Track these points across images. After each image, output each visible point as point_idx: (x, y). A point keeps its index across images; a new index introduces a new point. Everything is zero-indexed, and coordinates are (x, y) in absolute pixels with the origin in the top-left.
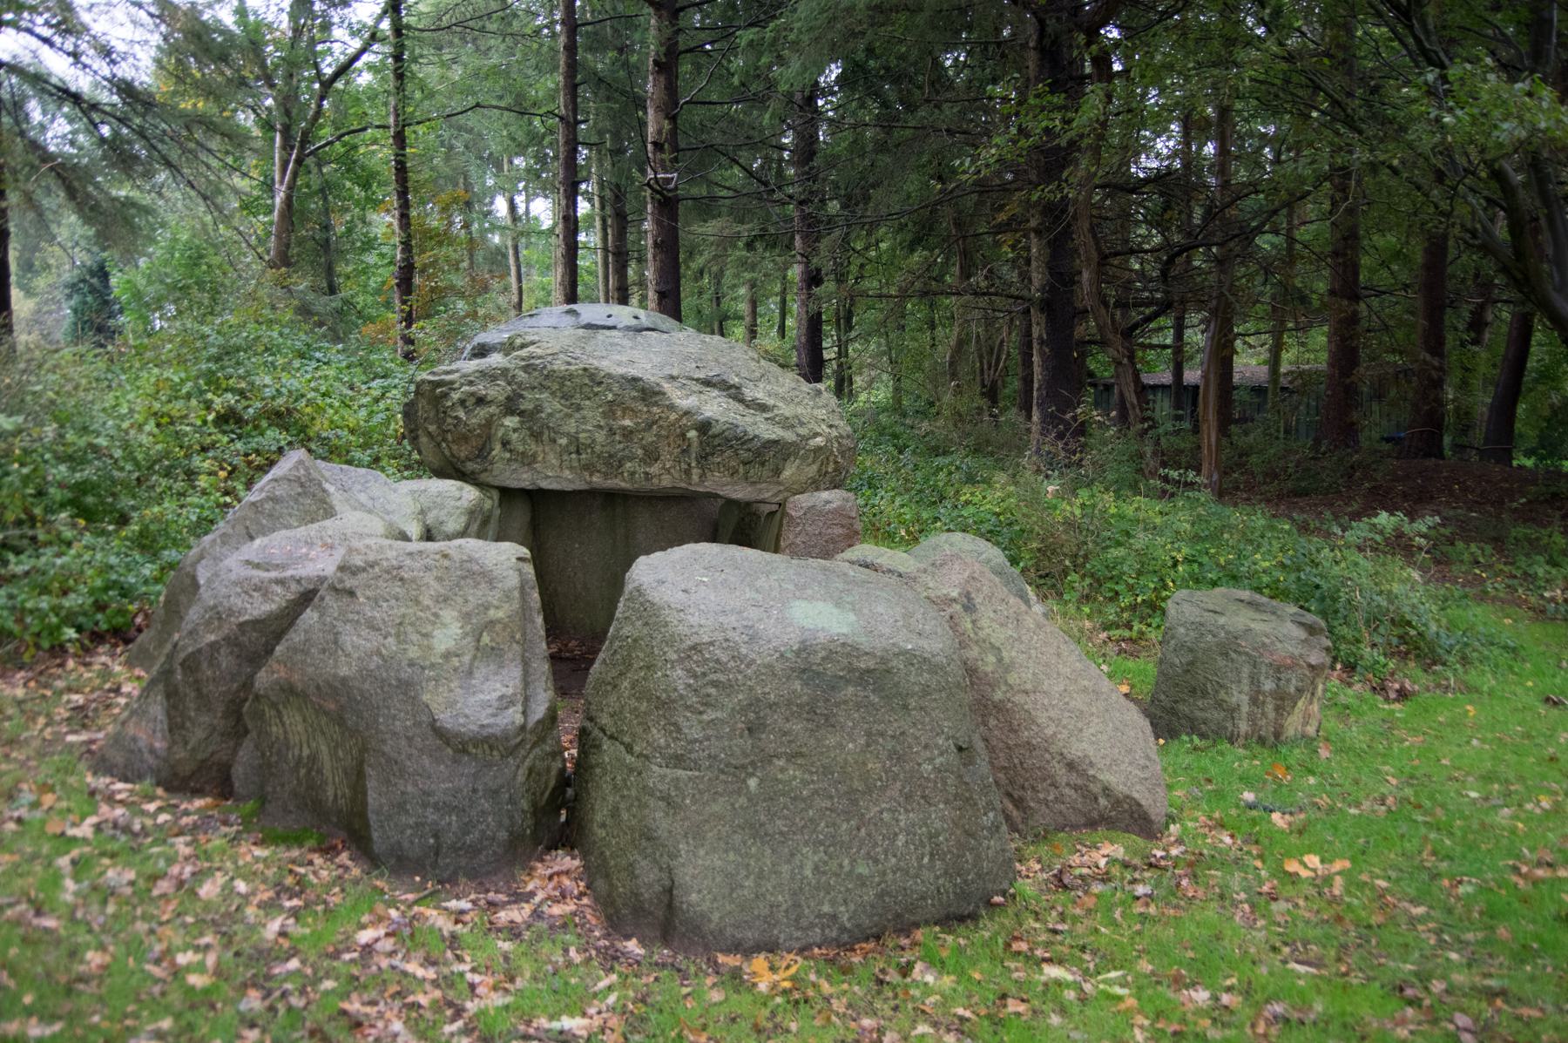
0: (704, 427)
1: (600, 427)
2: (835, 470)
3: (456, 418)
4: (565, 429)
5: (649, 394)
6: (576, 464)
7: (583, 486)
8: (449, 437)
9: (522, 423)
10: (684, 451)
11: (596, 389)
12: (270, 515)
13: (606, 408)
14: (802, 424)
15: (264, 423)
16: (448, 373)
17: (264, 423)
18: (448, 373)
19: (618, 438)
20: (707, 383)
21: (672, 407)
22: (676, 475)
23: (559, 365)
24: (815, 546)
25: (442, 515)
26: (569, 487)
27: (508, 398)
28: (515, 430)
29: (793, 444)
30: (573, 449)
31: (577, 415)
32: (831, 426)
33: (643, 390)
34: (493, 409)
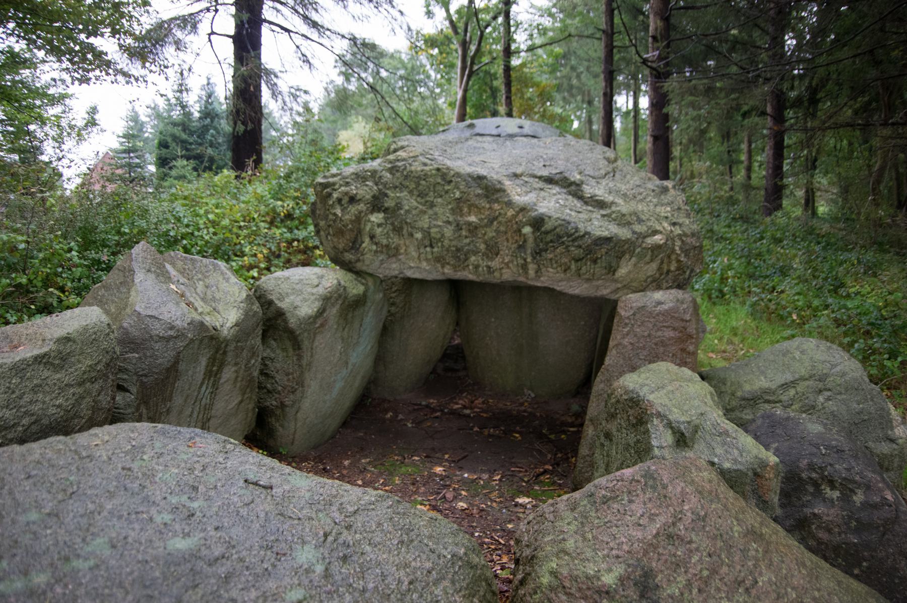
0: (538, 223)
1: (449, 222)
2: (678, 269)
3: (335, 214)
4: (420, 224)
5: (491, 191)
6: (430, 257)
9: (386, 219)
10: (520, 247)
11: (447, 188)
14: (640, 221)
19: (464, 233)
20: (549, 180)
21: (510, 204)
23: (417, 167)
24: (644, 348)
25: (298, 301)
28: (379, 225)
29: (627, 241)
30: (427, 242)
31: (430, 212)
32: (674, 224)
33: (486, 188)
34: (362, 207)
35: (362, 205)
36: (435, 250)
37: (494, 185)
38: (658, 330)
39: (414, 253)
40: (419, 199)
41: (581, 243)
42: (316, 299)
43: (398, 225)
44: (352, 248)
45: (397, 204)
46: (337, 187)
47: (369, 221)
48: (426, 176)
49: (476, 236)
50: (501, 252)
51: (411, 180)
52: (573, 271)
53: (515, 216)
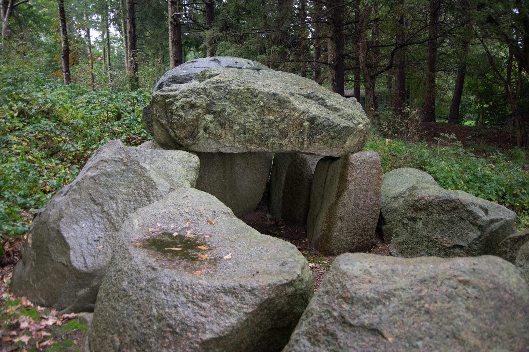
0: (312, 120)
1: (257, 120)
3: (179, 115)
4: (238, 121)
5: (282, 103)
7: (244, 151)
8: (175, 126)
9: (215, 118)
10: (301, 132)
11: (254, 100)
12: (106, 185)
13: (260, 110)
15: (40, 117)
16: (172, 91)
17: (40, 117)
18: (172, 91)
19: (266, 125)
20: (308, 97)
21: (295, 109)
22: (296, 145)
23: (234, 86)
26: (236, 151)
27: (208, 105)
28: (211, 122)
29: (353, 128)
30: (242, 131)
31: (244, 114)
33: (279, 100)
34: (200, 111)
35: (200, 110)
36: (248, 135)
37: (284, 99)
38: (371, 170)
39: (230, 138)
40: (236, 106)
41: (335, 129)
42: (193, 170)
43: (223, 121)
44: (191, 136)
45: (222, 110)
46: (178, 98)
47: (205, 119)
48: (241, 93)
49: (272, 127)
50: (289, 136)
51: (232, 95)
52: (329, 144)
53: (299, 116)
